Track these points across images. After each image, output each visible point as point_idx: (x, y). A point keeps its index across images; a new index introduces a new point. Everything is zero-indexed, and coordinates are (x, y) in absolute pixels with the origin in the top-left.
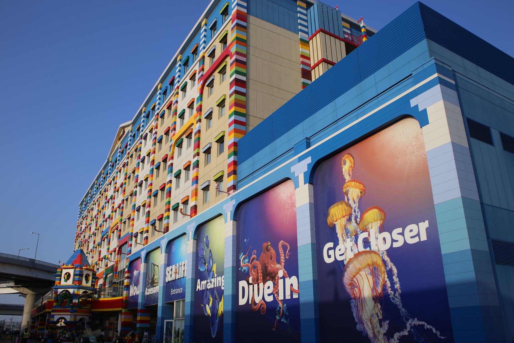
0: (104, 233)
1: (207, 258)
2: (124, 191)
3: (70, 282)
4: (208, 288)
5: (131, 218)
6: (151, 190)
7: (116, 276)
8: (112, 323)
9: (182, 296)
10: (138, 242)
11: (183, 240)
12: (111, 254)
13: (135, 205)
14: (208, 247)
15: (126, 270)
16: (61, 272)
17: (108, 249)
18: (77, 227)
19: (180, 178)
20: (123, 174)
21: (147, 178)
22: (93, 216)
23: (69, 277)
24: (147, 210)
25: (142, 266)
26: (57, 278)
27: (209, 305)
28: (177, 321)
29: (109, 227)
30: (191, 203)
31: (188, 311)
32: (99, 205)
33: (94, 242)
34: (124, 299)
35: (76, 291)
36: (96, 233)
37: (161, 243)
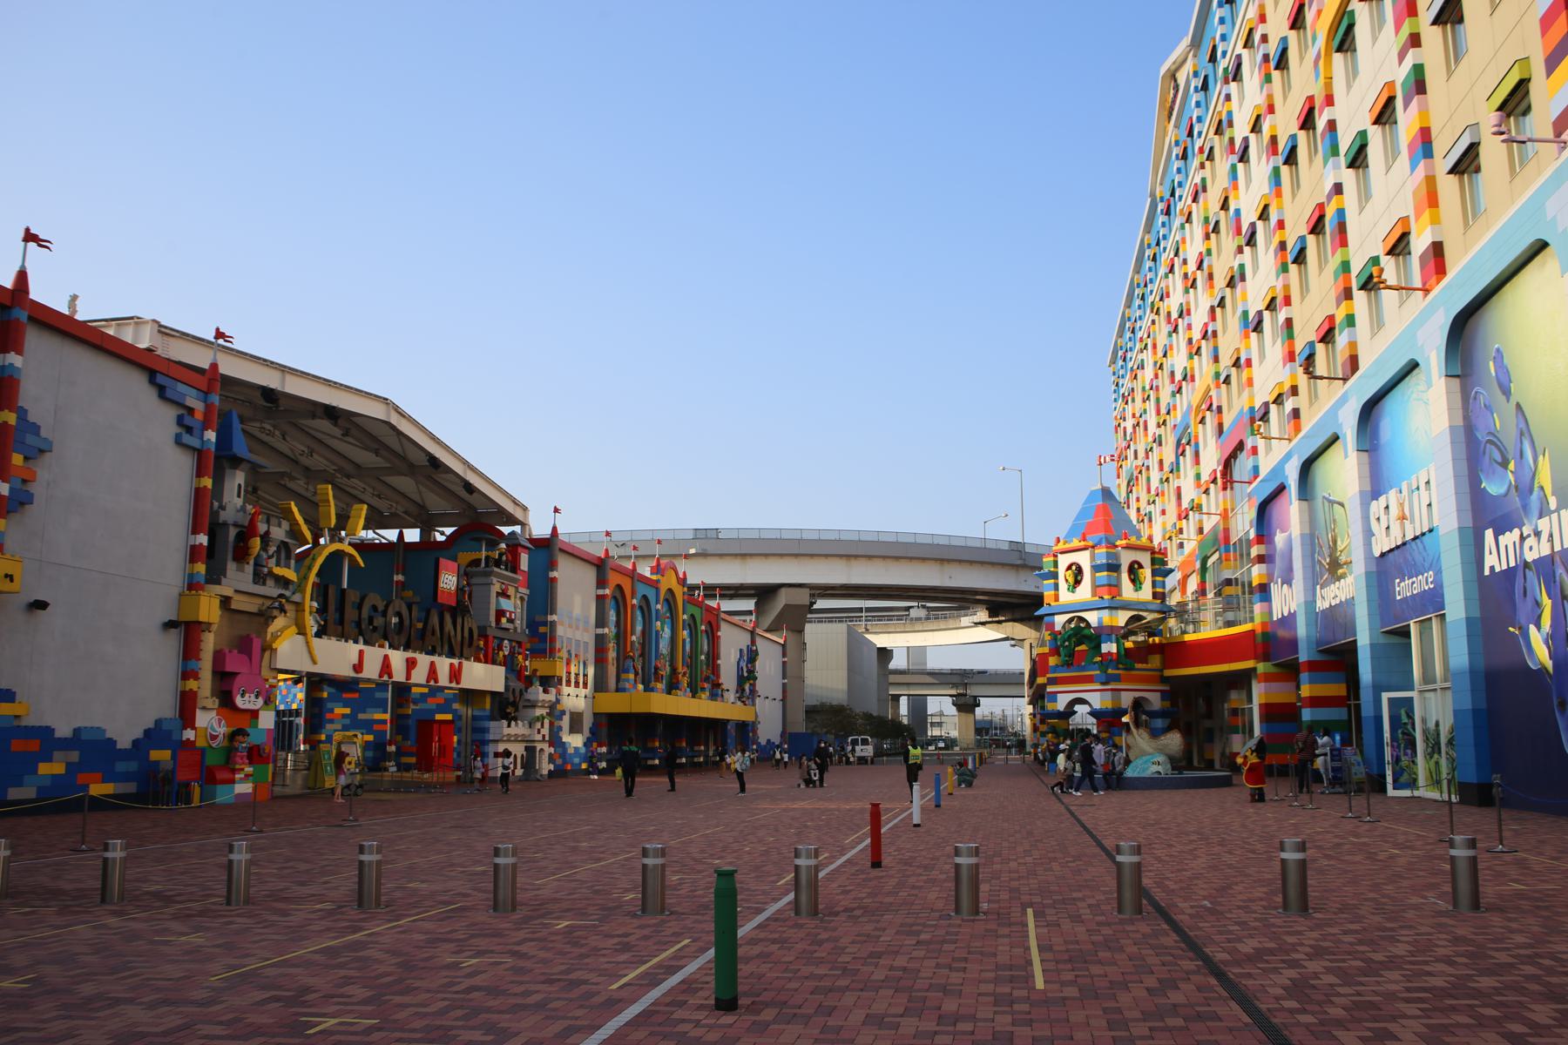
0: (1179, 430)
1: (1509, 440)
2: (1211, 276)
3: (1084, 592)
4: (1530, 557)
5: (1243, 361)
6: (1282, 246)
7: (1228, 560)
8: (1237, 709)
9: (1432, 601)
10: (1275, 432)
11: (1412, 392)
12: (1206, 492)
13: (1245, 313)
14: (1506, 392)
15: (1252, 535)
16: (1056, 564)
17: (1198, 476)
18: (1114, 430)
19: (1367, 166)
20: (1267, 250)
21: (1266, 207)
22: (1147, 387)
23: (1079, 578)
24: (1282, 316)
25: (1292, 511)
26: (1045, 582)
27: (1538, 627)
28: (1428, 695)
29: (1190, 407)
30: (1420, 243)
31: (1460, 656)
32: (1155, 346)
33: (1161, 462)
34: (1259, 630)
35: (1105, 614)
36: (1160, 436)
37: (1340, 421)
